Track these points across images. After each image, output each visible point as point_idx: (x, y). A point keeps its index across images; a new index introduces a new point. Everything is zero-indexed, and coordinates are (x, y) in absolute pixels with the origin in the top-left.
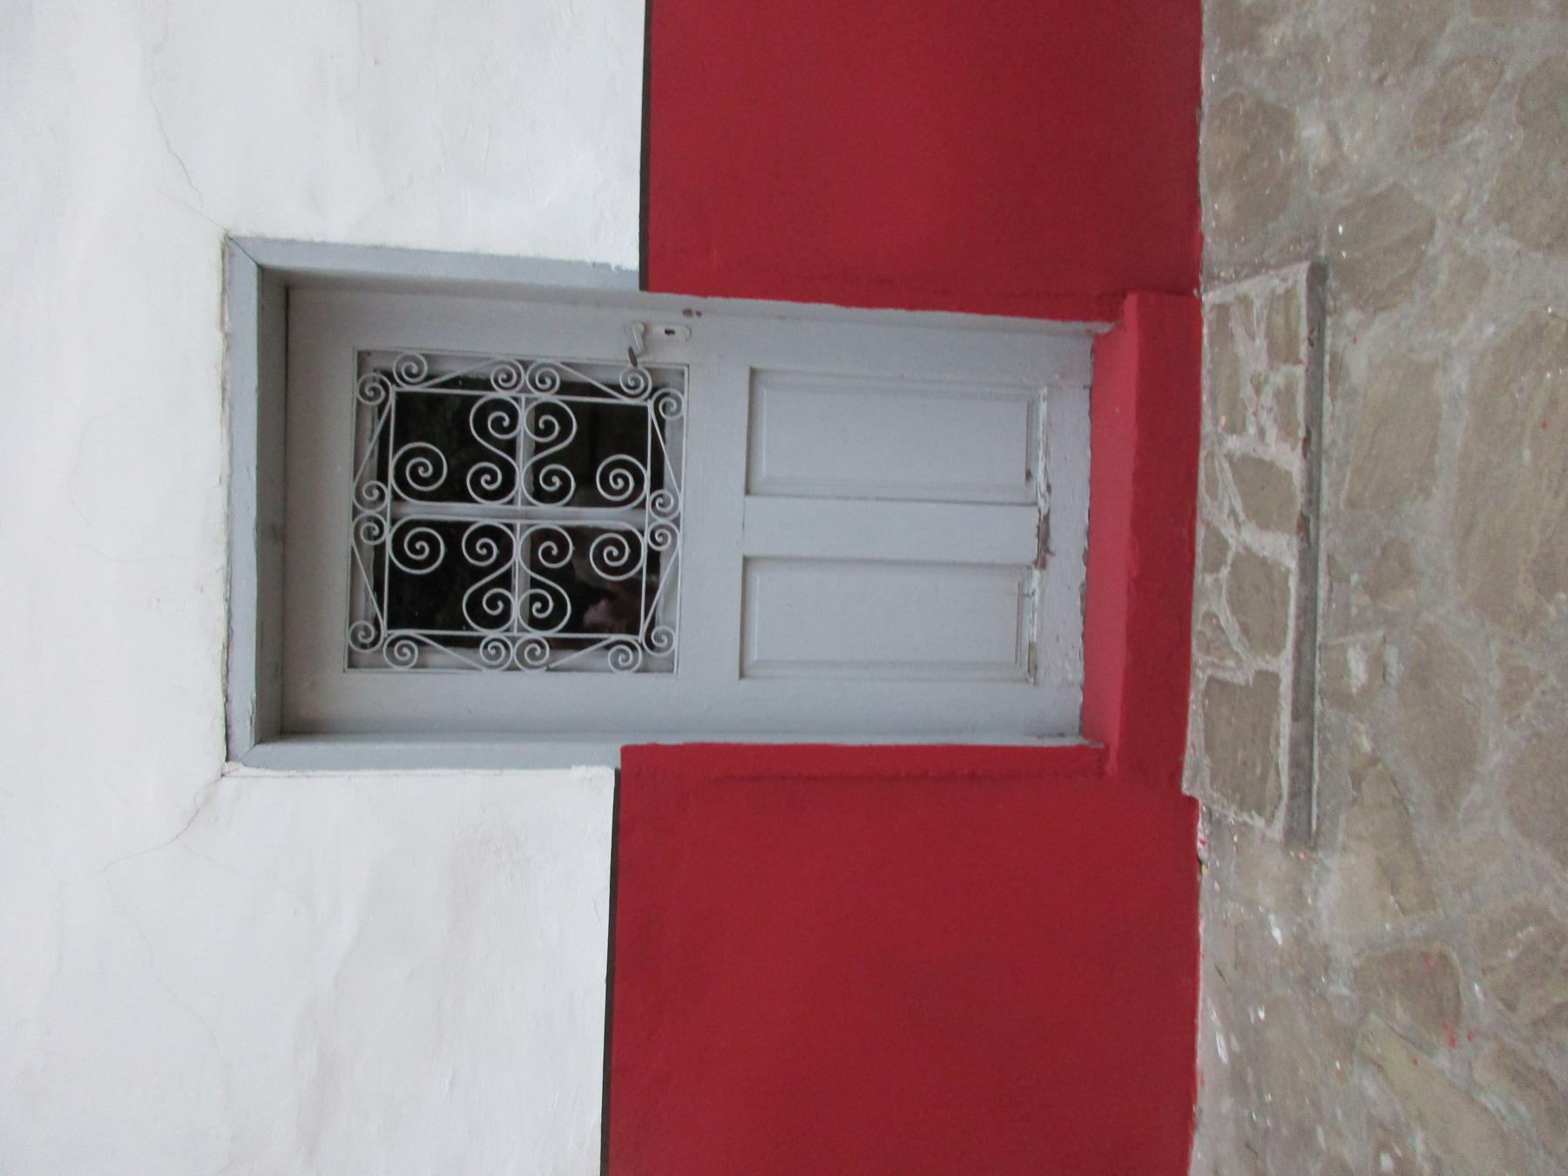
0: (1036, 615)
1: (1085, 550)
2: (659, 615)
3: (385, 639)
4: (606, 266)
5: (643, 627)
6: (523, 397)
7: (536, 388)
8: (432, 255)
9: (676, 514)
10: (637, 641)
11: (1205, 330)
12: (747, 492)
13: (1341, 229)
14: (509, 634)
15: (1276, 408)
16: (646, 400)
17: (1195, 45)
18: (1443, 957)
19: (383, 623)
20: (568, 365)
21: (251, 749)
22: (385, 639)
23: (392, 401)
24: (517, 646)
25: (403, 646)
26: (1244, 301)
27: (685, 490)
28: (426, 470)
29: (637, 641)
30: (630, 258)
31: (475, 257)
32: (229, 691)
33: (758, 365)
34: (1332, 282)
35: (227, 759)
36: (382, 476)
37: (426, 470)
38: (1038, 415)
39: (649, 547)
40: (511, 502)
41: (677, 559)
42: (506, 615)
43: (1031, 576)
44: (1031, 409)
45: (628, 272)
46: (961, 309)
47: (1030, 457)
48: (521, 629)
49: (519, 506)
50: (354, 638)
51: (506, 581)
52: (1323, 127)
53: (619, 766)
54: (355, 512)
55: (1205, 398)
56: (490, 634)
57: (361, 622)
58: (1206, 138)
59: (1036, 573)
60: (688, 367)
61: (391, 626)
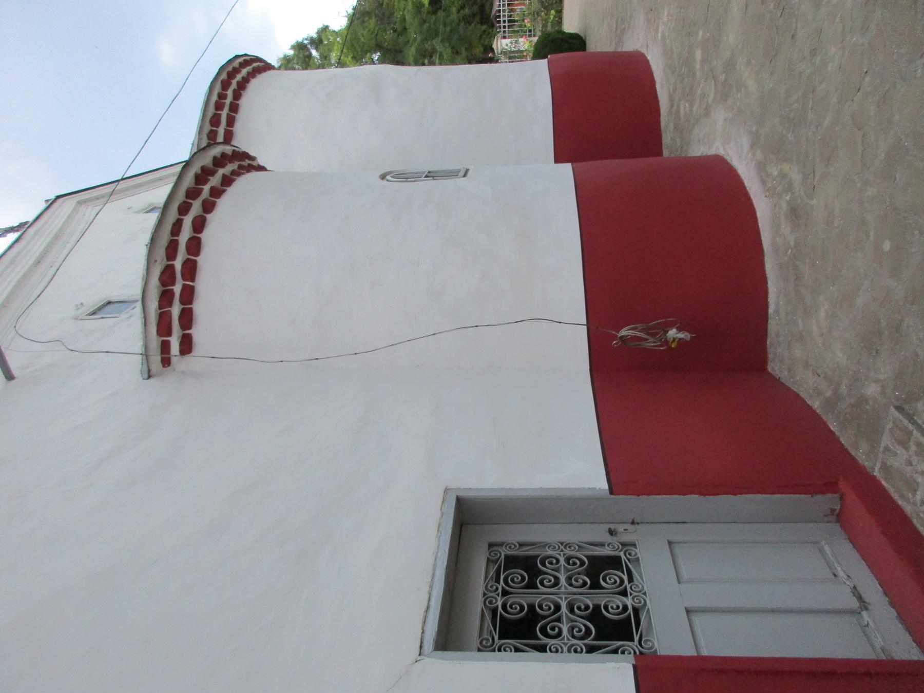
0: (876, 632)
1: (888, 601)
2: (644, 634)
3: (497, 645)
4: (595, 489)
5: (636, 638)
6: (562, 553)
7: (558, 644)
8: (524, 490)
9: (644, 591)
10: (634, 645)
11: (883, 483)
12: (679, 582)
13: (897, 394)
14: (563, 641)
15: (919, 458)
16: (620, 551)
17: (824, 424)
18: (767, 28)
19: (496, 637)
20: (580, 542)
21: (432, 652)
22: (497, 645)
23: (503, 557)
24: (567, 646)
25: (506, 647)
26: (887, 449)
27: (646, 582)
28: (518, 579)
29: (634, 645)
30: (603, 485)
31: (541, 489)
32: (425, 629)
33: (671, 539)
34: (907, 407)
35: (420, 655)
36: (498, 581)
37: (518, 579)
38: (826, 553)
39: (632, 605)
40: (559, 589)
41: (648, 610)
42: (560, 634)
43: (862, 617)
44: (821, 551)
45: (606, 489)
46: (759, 493)
47: (831, 567)
48: (568, 639)
49: (563, 590)
50: (481, 643)
51: (559, 620)
52: (873, 385)
53: (634, 663)
54: (484, 594)
55: (900, 503)
56: (552, 641)
57: (485, 636)
58: (843, 441)
59: (864, 613)
60: (637, 540)
61: (500, 638)
